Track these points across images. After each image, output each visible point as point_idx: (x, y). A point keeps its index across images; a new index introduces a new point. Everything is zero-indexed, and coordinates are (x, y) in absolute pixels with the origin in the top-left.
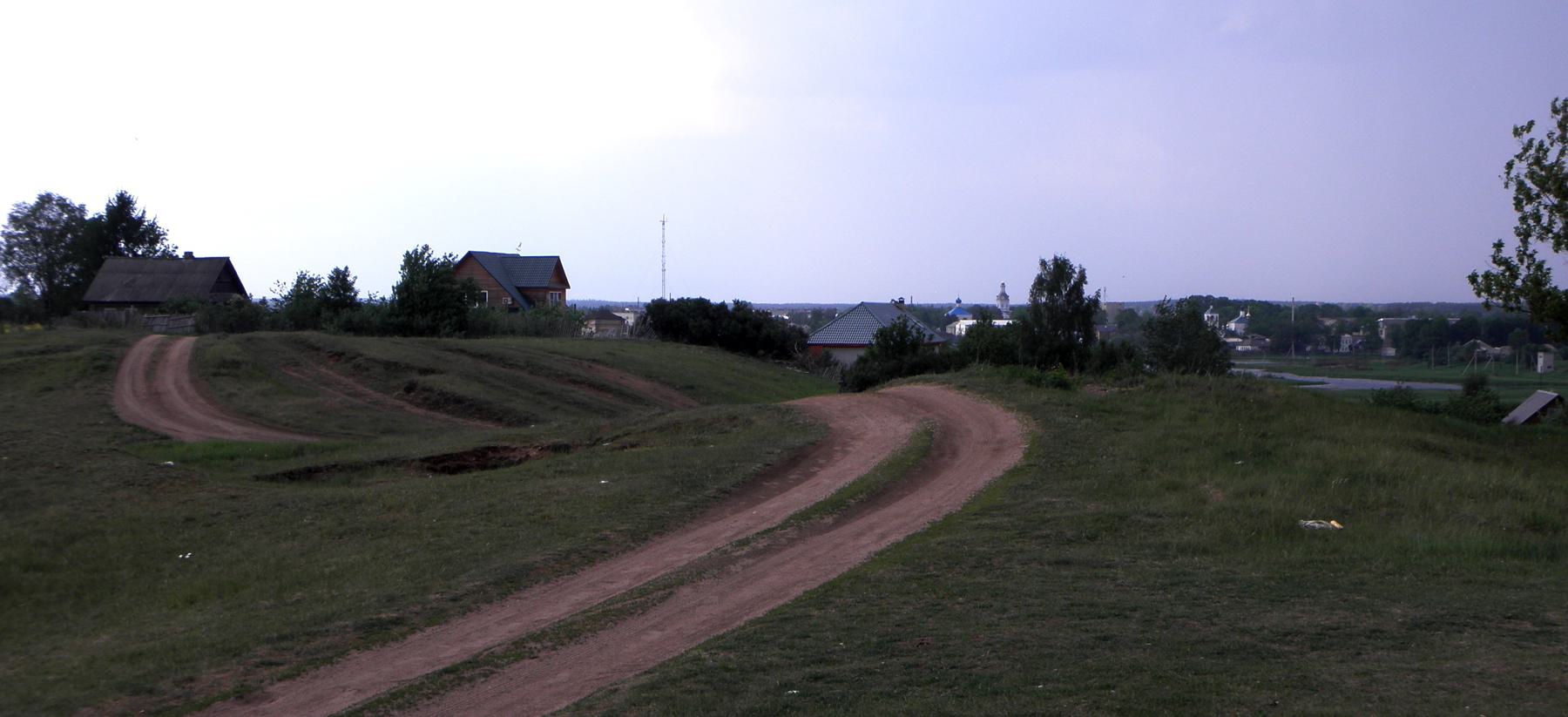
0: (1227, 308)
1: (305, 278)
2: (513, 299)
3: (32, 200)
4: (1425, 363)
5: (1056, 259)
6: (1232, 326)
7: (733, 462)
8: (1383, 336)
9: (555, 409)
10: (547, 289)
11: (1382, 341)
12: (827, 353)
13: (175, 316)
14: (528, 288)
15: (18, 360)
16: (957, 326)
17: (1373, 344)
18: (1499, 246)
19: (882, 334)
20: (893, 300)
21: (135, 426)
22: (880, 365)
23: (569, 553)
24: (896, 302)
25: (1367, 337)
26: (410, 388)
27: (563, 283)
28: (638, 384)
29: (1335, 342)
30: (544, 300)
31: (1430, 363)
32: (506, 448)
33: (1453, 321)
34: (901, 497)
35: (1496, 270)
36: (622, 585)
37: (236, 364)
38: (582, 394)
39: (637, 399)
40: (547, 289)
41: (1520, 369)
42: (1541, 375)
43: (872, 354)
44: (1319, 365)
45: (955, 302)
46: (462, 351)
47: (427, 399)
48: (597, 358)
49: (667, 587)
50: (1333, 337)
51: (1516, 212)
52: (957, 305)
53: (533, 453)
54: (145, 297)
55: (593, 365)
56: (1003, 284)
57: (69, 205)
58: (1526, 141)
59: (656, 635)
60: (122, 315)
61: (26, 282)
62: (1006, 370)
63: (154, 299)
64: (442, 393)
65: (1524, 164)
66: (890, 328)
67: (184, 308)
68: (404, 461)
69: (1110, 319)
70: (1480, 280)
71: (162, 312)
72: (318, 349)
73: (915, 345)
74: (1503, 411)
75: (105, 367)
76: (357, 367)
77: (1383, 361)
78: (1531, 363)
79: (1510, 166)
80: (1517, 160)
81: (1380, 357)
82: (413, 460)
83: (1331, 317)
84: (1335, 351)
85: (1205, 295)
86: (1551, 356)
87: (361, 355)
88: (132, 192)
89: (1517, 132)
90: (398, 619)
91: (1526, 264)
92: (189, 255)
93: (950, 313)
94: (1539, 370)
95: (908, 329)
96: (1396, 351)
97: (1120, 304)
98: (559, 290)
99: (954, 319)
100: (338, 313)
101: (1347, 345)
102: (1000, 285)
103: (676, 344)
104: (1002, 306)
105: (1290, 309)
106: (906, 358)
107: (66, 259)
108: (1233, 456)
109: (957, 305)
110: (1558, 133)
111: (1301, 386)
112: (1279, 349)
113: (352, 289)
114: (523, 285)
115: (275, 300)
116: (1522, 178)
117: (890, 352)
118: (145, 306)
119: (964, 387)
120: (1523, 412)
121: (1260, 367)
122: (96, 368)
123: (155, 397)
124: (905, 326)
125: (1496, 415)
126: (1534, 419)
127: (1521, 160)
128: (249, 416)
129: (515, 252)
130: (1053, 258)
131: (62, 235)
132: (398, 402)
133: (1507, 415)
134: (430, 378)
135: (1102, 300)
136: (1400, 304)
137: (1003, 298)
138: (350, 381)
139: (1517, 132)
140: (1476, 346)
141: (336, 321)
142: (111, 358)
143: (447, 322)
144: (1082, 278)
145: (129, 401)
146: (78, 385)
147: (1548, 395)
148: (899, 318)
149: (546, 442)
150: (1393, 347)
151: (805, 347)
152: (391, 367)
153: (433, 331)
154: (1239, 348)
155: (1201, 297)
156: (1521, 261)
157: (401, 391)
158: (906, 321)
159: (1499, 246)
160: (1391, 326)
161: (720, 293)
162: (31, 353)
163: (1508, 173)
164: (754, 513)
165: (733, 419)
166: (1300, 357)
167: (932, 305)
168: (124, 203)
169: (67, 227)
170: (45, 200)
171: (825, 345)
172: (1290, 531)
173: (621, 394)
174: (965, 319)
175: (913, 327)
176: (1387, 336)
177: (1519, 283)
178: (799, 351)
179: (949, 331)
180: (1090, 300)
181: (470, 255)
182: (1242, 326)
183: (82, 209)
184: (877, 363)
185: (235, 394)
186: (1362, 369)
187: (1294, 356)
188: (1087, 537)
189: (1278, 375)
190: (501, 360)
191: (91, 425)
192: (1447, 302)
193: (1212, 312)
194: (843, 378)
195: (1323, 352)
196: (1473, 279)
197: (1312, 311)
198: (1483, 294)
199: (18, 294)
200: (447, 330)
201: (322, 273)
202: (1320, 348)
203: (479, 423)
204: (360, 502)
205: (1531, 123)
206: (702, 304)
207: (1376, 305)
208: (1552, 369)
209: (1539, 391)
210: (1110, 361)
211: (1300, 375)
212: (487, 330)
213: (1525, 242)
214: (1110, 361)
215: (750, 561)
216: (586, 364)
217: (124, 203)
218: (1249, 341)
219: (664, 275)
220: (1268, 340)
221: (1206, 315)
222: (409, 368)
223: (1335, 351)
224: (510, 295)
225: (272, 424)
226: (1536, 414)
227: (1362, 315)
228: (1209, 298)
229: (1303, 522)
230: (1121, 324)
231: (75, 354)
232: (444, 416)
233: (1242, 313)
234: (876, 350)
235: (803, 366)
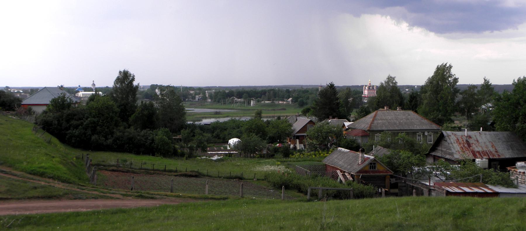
5: (124, 71)
8: (207, 96)
11: (207, 97)
12: (30, 107)
16: (79, 94)
17: (204, 98)
19: (54, 101)
20: (58, 86)
22: (53, 114)
24: (60, 87)
25: (203, 96)
29: (194, 98)
31: (222, 104)
33: (227, 91)
41: (246, 105)
42: (253, 107)
43: (49, 109)
44: (191, 105)
45: (78, 86)
50: (194, 96)
52: (79, 87)
56: (93, 81)
66: (58, 99)
73: (69, 105)
78: (249, 103)
81: (207, 102)
84: (194, 100)
85: (155, 84)
86: (255, 102)
93: (77, 90)
95: (65, 99)
96: (211, 100)
99: (78, 92)
101: (197, 99)
102: (92, 81)
104: (93, 87)
106: (65, 111)
109: (79, 87)
111: (189, 111)
117: (57, 108)
124: (64, 97)
130: (123, 70)
135: (140, 85)
137: (94, 85)
144: (133, 79)
148: (61, 94)
150: (210, 99)
151: (20, 105)
155: (154, 85)
158: (64, 95)
160: (209, 93)
167: (71, 87)
174: (82, 92)
175: (68, 98)
176: (208, 96)
178: (17, 107)
179: (76, 95)
184: (51, 114)
186: (203, 106)
192: (287, 85)
194: (36, 120)
195: (191, 100)
202: (190, 100)
208: (255, 105)
221: (156, 90)
223: (194, 100)
227: (200, 90)
228: (157, 85)
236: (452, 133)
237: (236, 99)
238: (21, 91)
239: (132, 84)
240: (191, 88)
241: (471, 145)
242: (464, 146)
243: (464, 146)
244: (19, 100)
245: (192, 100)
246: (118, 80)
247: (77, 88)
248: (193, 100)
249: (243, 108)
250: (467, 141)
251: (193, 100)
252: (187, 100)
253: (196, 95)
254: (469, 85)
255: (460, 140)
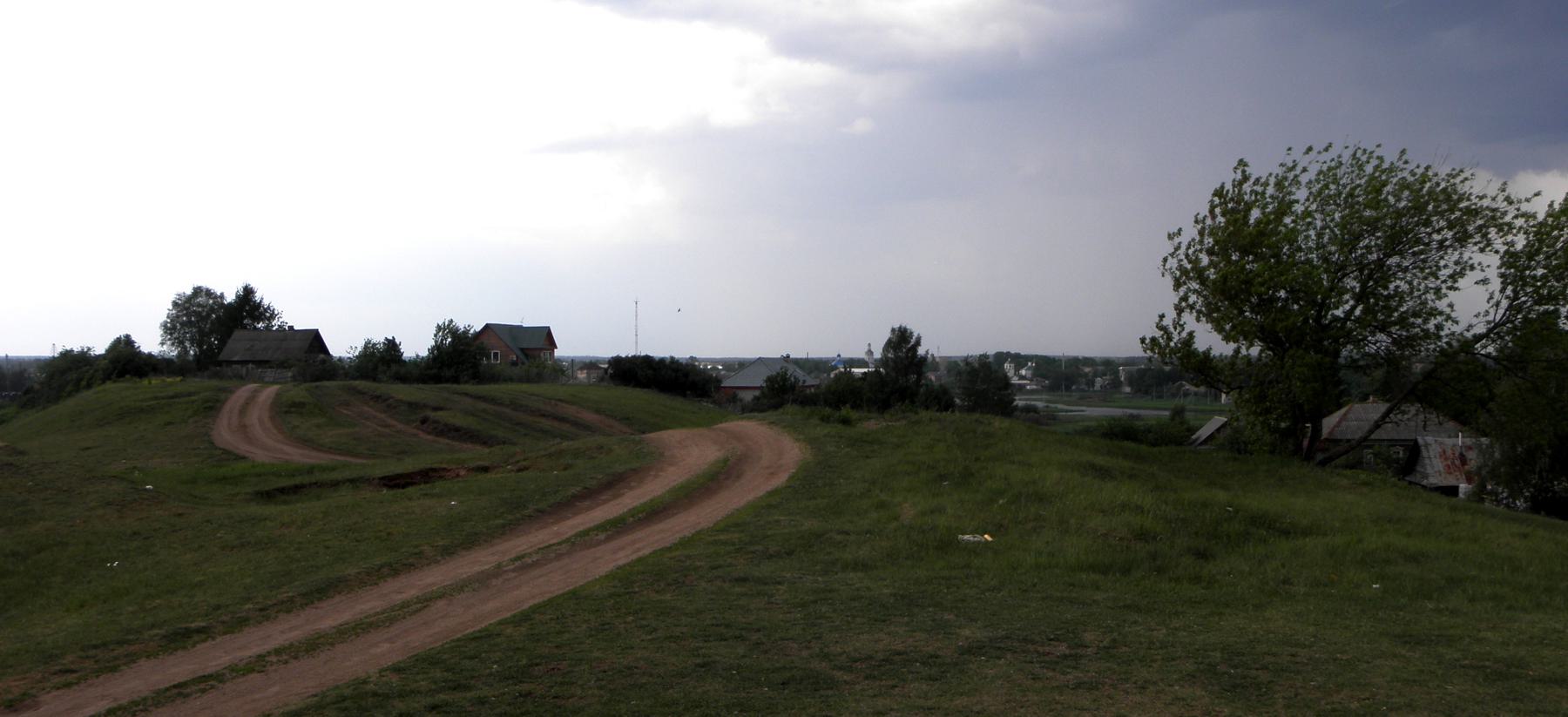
0: (1019, 360)
1: (370, 343)
2: (517, 357)
3: (189, 292)
4: (1150, 397)
5: (900, 328)
6: (1023, 372)
7: (559, 486)
8: (1122, 379)
9: (526, 435)
10: (541, 349)
12: (734, 393)
13: (279, 371)
14: (528, 349)
15: (152, 402)
17: (1116, 384)
18: (1162, 317)
19: (770, 380)
21: (224, 450)
23: (382, 566)
26: (424, 421)
27: (551, 343)
28: (589, 416)
29: (1091, 383)
30: (539, 356)
32: (444, 469)
34: (674, 515)
35: (1158, 334)
36: (412, 593)
37: (302, 405)
38: (546, 423)
39: (588, 428)
40: (541, 349)
43: (763, 393)
46: (466, 394)
47: (435, 428)
48: (562, 398)
49: (426, 601)
51: (162, 310)
53: (463, 473)
54: (259, 358)
55: (559, 403)
57: (212, 294)
58: (1176, 244)
59: (386, 646)
60: (244, 371)
61: (185, 348)
62: (808, 409)
63: (266, 359)
64: (446, 425)
65: (1175, 260)
67: (286, 365)
68: (367, 480)
69: (942, 368)
70: (1147, 341)
71: (271, 367)
72: (364, 393)
74: (1192, 430)
75: (212, 407)
76: (389, 406)
77: (1123, 396)
78: (1218, 398)
79: (1165, 260)
80: (1170, 258)
82: (373, 479)
83: (1088, 366)
84: (1091, 389)
87: (392, 398)
88: (253, 285)
89: (1171, 237)
90: (204, 627)
91: (1178, 331)
92: (291, 328)
93: (833, 364)
94: (1223, 401)
97: (949, 357)
98: (548, 350)
100: (389, 367)
103: (625, 388)
105: (1061, 360)
107: (211, 332)
108: (942, 477)
110: (1198, 238)
112: (1053, 388)
113: (399, 351)
114: (525, 346)
115: (349, 358)
116: (1174, 269)
118: (261, 363)
119: (773, 423)
120: (1204, 432)
121: (1041, 400)
122: (205, 408)
123: (243, 428)
124: (786, 374)
125: (1187, 433)
126: (1211, 437)
127: (1173, 257)
128: (305, 442)
129: (520, 324)
131: (209, 315)
132: (415, 431)
133: (1194, 434)
134: (440, 413)
136: (1134, 358)
138: (383, 416)
139: (1171, 237)
140: (1182, 385)
141: (388, 374)
142: (217, 401)
143: (465, 373)
144: (918, 343)
145: (224, 432)
146: (191, 420)
147: (1222, 420)
149: (472, 465)
151: (719, 388)
152: (413, 406)
153: (456, 380)
154: (1028, 387)
156: (1175, 328)
157: (418, 423)
158: (787, 370)
159: (1162, 317)
161: (658, 351)
162: (163, 398)
163: (1164, 266)
164: (556, 529)
165: (600, 448)
166: (1068, 393)
167: (821, 359)
168: (248, 292)
169: (212, 310)
170: (198, 291)
171: (733, 388)
172: (947, 544)
173: (576, 424)
176: (1125, 379)
177: (1172, 344)
180: (922, 357)
181: (487, 327)
182: (1030, 372)
183: (222, 296)
185: (298, 426)
187: (1064, 393)
188: (786, 553)
189: (1053, 405)
190: (492, 400)
191: (194, 449)
193: (1010, 363)
196: (1143, 340)
197: (1076, 362)
198: (1148, 351)
199: (179, 356)
200: (466, 378)
201: (379, 338)
203: (470, 446)
204: (265, 519)
205: (1180, 230)
206: (647, 360)
207: (1119, 358)
209: (1216, 417)
210: (941, 400)
211: (1069, 405)
212: (494, 378)
213: (1179, 315)
214: (941, 400)
215: (513, 575)
216: (553, 402)
217: (248, 292)
218: (1033, 383)
219: (637, 339)
220: (1047, 382)
222: (425, 406)
223: (1091, 389)
224: (515, 354)
225: (319, 448)
226: (1212, 433)
228: (1008, 354)
229: (960, 536)
230: (949, 371)
231: (193, 398)
232: (447, 441)
233: (1029, 364)
234: (766, 390)
235: (714, 402)
236: (1436, 441)
237: (1187, 387)
238: (720, 367)
239: (916, 351)
240: (1088, 361)
241: (1468, 462)
242: (1453, 463)
243: (1453, 463)
244: (718, 381)
245: (1087, 389)
246: (890, 345)
247: (834, 359)
248: (1089, 387)
249: (1201, 407)
250: (1462, 455)
251: (1089, 387)
252: (1074, 387)
253: (1096, 375)
254: (627, 357)
255: (1449, 452)
